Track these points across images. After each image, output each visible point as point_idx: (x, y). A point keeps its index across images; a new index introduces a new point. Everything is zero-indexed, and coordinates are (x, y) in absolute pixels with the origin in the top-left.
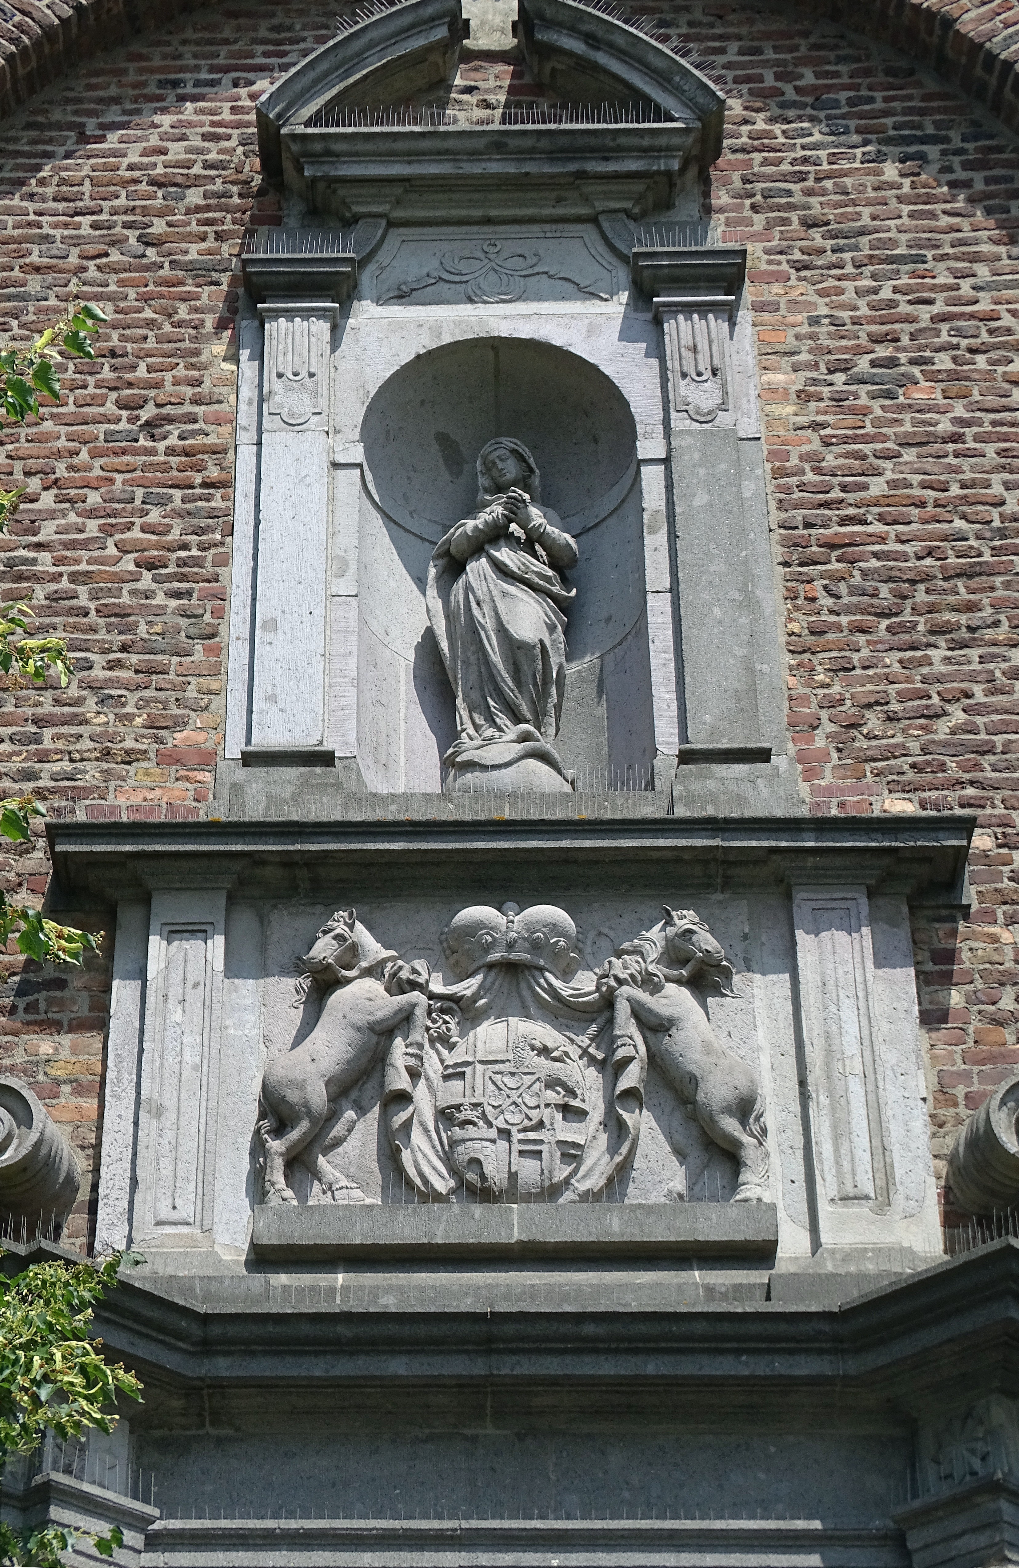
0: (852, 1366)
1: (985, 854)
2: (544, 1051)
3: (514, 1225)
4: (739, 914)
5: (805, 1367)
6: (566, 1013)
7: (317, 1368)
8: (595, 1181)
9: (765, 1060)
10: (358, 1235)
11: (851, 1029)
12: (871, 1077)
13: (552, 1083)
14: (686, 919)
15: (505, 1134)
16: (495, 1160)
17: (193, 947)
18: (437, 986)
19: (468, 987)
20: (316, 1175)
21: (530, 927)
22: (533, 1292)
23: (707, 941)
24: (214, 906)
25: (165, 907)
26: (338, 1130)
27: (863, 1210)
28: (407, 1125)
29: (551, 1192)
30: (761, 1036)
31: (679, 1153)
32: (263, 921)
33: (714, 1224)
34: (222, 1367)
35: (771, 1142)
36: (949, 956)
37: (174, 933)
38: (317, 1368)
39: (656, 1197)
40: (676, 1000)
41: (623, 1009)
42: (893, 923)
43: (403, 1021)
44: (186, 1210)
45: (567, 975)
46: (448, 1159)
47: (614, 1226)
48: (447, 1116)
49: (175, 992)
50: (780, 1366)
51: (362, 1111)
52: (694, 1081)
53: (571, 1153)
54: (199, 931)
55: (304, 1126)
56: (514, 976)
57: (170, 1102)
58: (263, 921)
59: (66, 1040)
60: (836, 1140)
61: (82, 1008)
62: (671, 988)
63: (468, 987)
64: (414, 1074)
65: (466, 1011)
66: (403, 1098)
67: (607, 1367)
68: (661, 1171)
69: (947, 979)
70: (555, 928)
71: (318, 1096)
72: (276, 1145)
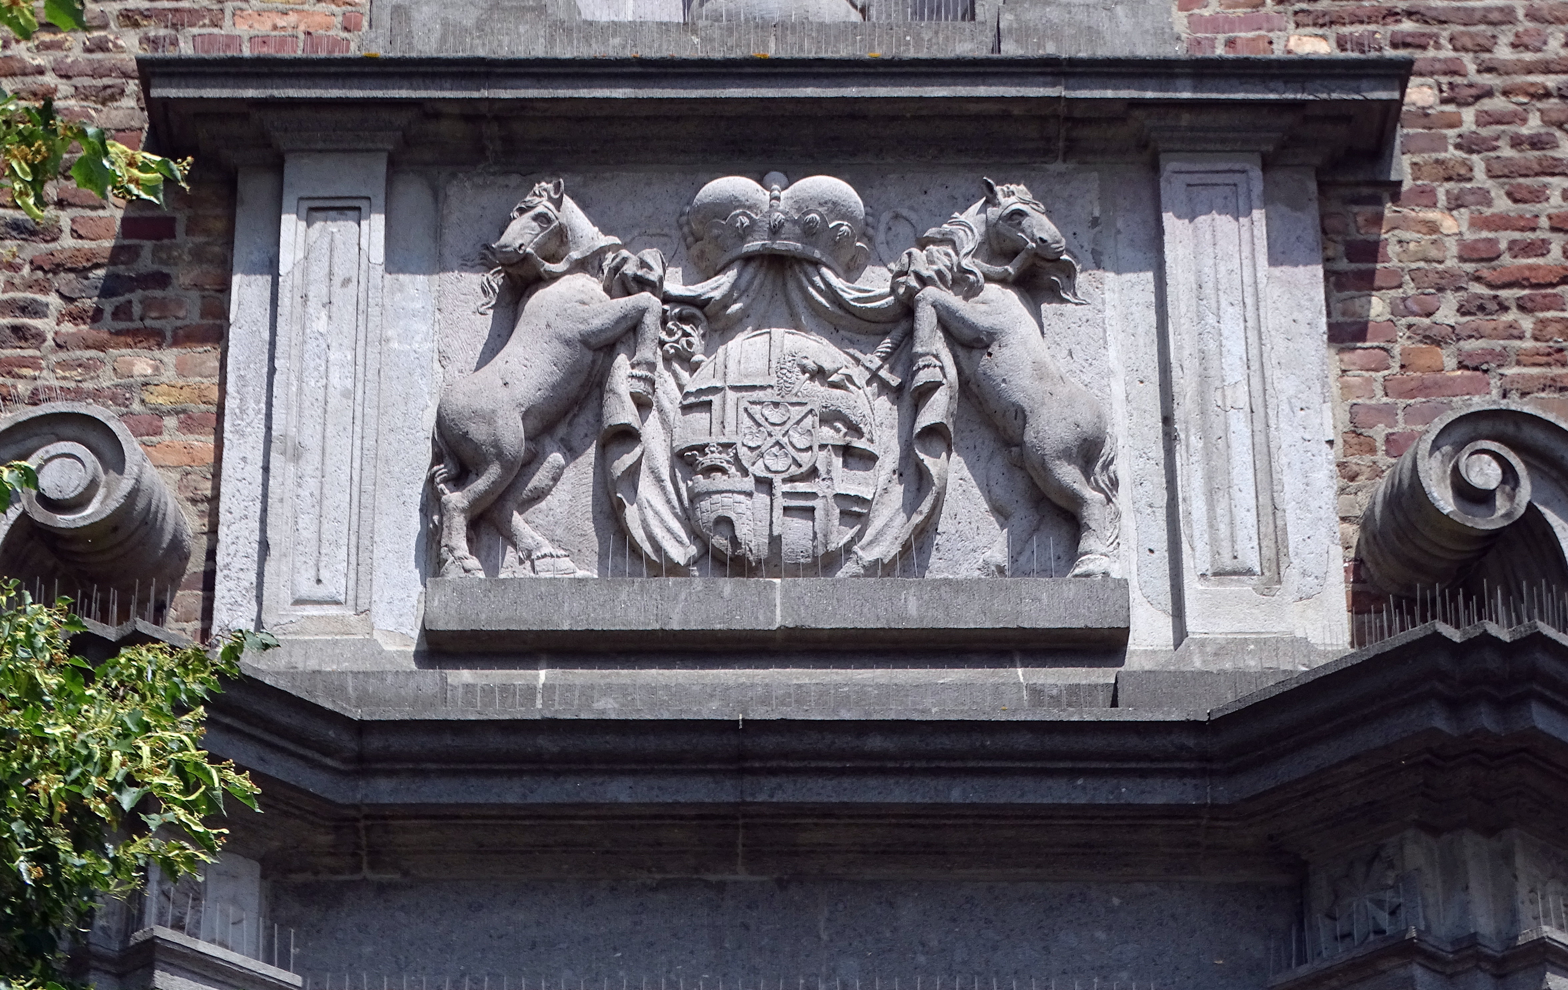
0: (1222, 792)
1: (1424, 113)
2: (819, 374)
3: (776, 605)
4: (1087, 192)
5: (1162, 793)
6: (850, 324)
7: (510, 793)
8: (885, 549)
9: (1118, 389)
10: (566, 619)
11: (1235, 347)
12: (1259, 413)
13: (830, 417)
14: (1014, 196)
15: (765, 484)
16: (752, 520)
17: (342, 229)
18: (675, 286)
19: (716, 287)
20: (510, 538)
21: (802, 206)
22: (800, 694)
23: (1042, 226)
24: (368, 174)
25: (304, 176)
26: (539, 478)
27: (1245, 588)
28: (633, 471)
29: (827, 562)
30: (1113, 356)
31: (1000, 512)
32: (437, 195)
33: (1045, 605)
34: (384, 791)
35: (1123, 498)
36: (1371, 251)
37: (315, 211)
38: (510, 793)
39: (968, 570)
40: (999, 306)
41: (926, 318)
42: (1295, 205)
43: (629, 330)
44: (335, 584)
45: (851, 272)
46: (688, 518)
47: (908, 608)
48: (686, 460)
49: (318, 291)
50: (1126, 792)
51: (572, 453)
52: (1021, 414)
53: (854, 511)
54: (349, 208)
55: (493, 472)
56: (780, 273)
57: (310, 438)
58: (437, 195)
59: (170, 356)
60: (1211, 494)
61: (190, 312)
62: (992, 290)
63: (716, 287)
64: (643, 404)
65: (714, 320)
66: (627, 436)
67: (899, 793)
68: (974, 535)
69: (1367, 282)
70: (835, 208)
71: (512, 433)
72: (456, 499)
